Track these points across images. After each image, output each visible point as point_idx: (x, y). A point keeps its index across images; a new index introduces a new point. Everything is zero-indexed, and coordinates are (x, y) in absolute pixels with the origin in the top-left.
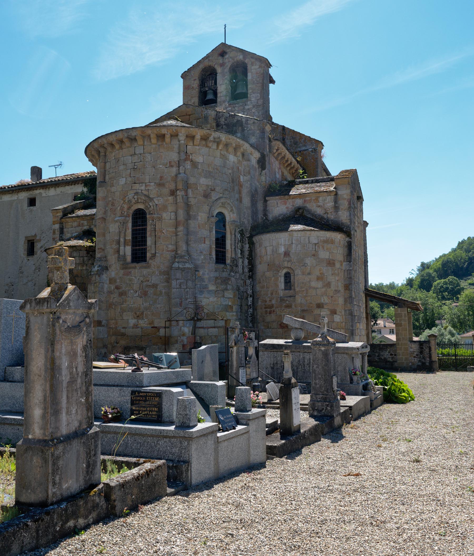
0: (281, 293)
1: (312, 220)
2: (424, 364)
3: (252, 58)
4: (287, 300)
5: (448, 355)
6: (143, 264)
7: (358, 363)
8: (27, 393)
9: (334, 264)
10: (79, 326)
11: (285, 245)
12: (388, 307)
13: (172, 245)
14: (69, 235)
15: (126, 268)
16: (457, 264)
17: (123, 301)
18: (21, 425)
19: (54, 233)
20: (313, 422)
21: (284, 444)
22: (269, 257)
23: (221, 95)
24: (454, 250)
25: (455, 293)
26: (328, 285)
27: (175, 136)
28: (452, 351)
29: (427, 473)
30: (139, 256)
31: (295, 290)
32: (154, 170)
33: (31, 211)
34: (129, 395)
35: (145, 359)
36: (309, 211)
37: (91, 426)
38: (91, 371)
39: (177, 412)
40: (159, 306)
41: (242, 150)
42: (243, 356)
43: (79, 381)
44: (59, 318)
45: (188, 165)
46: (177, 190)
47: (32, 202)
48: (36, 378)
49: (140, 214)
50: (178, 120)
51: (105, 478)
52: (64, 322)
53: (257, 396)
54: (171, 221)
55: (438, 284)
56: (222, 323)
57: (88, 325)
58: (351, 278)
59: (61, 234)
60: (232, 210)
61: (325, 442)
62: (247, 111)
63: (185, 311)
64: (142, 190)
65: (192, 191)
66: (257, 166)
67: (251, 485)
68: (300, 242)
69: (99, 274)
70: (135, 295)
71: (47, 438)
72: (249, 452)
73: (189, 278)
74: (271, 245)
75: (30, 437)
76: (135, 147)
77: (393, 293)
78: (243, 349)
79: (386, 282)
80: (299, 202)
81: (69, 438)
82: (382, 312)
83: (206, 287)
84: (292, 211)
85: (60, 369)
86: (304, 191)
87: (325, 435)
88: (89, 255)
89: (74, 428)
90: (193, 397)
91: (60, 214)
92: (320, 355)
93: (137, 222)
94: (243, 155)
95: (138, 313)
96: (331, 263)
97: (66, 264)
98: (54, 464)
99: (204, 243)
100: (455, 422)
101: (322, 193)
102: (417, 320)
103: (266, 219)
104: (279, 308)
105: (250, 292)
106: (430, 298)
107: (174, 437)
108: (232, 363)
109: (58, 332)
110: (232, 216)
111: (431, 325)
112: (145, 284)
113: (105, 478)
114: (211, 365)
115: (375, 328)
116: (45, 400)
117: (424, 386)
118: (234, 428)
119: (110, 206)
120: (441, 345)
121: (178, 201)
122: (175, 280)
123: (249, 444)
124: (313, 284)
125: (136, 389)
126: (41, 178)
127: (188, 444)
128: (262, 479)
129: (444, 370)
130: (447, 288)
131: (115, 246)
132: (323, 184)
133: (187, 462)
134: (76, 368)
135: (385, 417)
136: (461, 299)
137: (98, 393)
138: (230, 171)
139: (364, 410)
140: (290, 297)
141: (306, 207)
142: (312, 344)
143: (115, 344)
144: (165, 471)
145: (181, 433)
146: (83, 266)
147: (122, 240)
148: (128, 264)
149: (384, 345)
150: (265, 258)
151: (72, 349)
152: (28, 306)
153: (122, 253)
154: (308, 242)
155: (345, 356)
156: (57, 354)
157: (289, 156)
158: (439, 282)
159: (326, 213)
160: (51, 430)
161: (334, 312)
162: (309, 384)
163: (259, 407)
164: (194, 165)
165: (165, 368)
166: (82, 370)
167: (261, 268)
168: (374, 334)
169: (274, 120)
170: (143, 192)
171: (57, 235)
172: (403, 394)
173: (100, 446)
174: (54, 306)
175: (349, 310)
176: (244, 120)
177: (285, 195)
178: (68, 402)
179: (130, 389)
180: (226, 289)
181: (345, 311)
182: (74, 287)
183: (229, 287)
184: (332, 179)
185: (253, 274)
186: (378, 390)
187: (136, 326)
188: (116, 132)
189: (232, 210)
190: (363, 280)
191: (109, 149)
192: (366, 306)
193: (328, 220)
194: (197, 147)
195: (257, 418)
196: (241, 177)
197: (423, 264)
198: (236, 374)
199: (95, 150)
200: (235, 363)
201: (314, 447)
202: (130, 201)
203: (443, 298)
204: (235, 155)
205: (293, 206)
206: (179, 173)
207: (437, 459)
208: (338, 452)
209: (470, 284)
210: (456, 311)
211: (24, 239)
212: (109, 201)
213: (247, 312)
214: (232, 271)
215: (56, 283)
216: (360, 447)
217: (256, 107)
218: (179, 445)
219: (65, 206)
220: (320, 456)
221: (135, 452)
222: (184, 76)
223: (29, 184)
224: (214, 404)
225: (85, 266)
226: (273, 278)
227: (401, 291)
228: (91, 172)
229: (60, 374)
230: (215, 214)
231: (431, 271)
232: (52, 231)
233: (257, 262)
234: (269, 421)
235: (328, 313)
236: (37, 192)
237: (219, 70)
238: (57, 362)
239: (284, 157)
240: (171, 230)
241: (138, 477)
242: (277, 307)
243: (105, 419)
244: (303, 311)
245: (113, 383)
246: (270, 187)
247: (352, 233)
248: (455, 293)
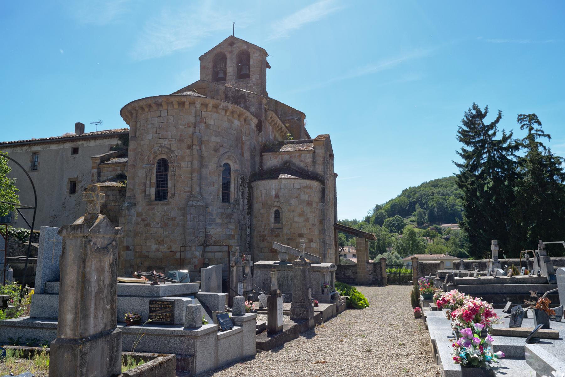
0: (272, 226)
1: (296, 171)
2: (376, 279)
5: (395, 273)
6: (165, 202)
7: (328, 279)
8: (61, 301)
9: (312, 204)
10: (107, 247)
11: (275, 189)
12: (352, 238)
14: (105, 178)
15: (151, 205)
16: (401, 206)
18: (56, 329)
19: (93, 176)
20: (293, 324)
21: (270, 340)
24: (399, 196)
25: (399, 228)
26: (307, 220)
27: (192, 103)
28: (397, 270)
29: (375, 360)
30: (161, 195)
32: (175, 129)
33: (74, 158)
34: (148, 303)
35: (162, 275)
36: (294, 164)
37: (114, 328)
38: (116, 284)
39: (186, 316)
41: (244, 116)
42: (241, 273)
43: (106, 291)
44: (90, 241)
45: (202, 126)
47: (75, 151)
48: (69, 289)
49: (163, 162)
50: (195, 92)
51: (124, 370)
52: (95, 244)
53: (251, 304)
55: (388, 221)
56: (226, 249)
57: (115, 247)
58: (324, 215)
60: (236, 162)
61: (302, 338)
62: (250, 88)
63: (197, 239)
66: (256, 129)
67: (243, 372)
69: (128, 209)
71: (76, 338)
72: (242, 347)
74: (266, 188)
75: (63, 337)
77: (355, 227)
78: (241, 268)
79: (351, 219)
80: (286, 158)
81: (95, 338)
82: (348, 241)
83: (214, 220)
85: (90, 282)
86: (290, 149)
87: (302, 334)
89: (100, 330)
90: (199, 304)
91: (98, 161)
92: (299, 273)
93: (160, 169)
94: (245, 120)
96: (309, 204)
97: (97, 198)
98: (82, 359)
100: (397, 322)
102: (373, 248)
103: (262, 169)
105: (248, 224)
106: (383, 231)
107: (183, 336)
108: (233, 279)
109: (89, 252)
111: (382, 251)
112: (165, 217)
113: (124, 370)
114: (216, 281)
115: (342, 253)
116: (76, 307)
117: (376, 296)
118: (231, 329)
120: (390, 266)
123: (243, 341)
124: (296, 219)
125: (153, 299)
126: (84, 132)
127: (194, 341)
128: (252, 368)
129: (391, 284)
130: (394, 224)
131: (142, 187)
132: (305, 144)
133: (193, 356)
134: (104, 281)
135: (347, 320)
136: (404, 232)
137: (123, 303)
138: (235, 132)
139: (331, 314)
140: (279, 228)
142: (293, 264)
144: (175, 363)
145: (189, 333)
147: (148, 182)
148: (152, 201)
149: (348, 266)
151: (100, 266)
152: (65, 231)
153: (147, 193)
155: (318, 273)
156: (88, 270)
157: (279, 122)
158: (388, 220)
159: (307, 166)
160: (80, 331)
161: (311, 240)
162: (291, 295)
163: (252, 312)
164: (207, 126)
165: (178, 282)
166: (108, 283)
167: (257, 206)
168: (341, 258)
169: (269, 96)
171: (95, 178)
172: (361, 302)
173: (121, 344)
174: (86, 232)
176: (246, 94)
177: (276, 152)
178: (96, 308)
179: (149, 299)
180: (230, 222)
181: (320, 239)
182: (104, 216)
183: (232, 221)
184: (311, 141)
185: (251, 211)
186: (342, 299)
187: (157, 251)
188: (146, 98)
189: (236, 162)
190: (333, 217)
191: (140, 111)
192: (335, 237)
193: (308, 171)
194: (210, 113)
195: (249, 321)
196: (243, 137)
197: (377, 206)
198: (235, 288)
199: (129, 112)
200: (234, 279)
201: (293, 343)
202: (155, 152)
203: (392, 231)
204: (239, 120)
206: (195, 132)
207: (383, 349)
208: (311, 346)
209: (410, 221)
210: (400, 241)
211: (67, 180)
213: (246, 240)
214: (234, 208)
215: (89, 214)
216: (328, 342)
218: (187, 342)
219: (103, 155)
220: (298, 349)
221: (151, 349)
222: (201, 58)
223: (73, 137)
224: (216, 310)
227: (362, 225)
228: (125, 129)
229: (90, 286)
230: (222, 164)
231: (383, 211)
232: (91, 174)
233: (255, 202)
234: (259, 323)
235: (307, 241)
236: (80, 143)
237: (228, 56)
238: (88, 276)
239: (276, 124)
241: (152, 368)
243: (128, 322)
244: (288, 239)
245: (135, 294)
246: (265, 145)
247: (325, 181)
248: (399, 228)
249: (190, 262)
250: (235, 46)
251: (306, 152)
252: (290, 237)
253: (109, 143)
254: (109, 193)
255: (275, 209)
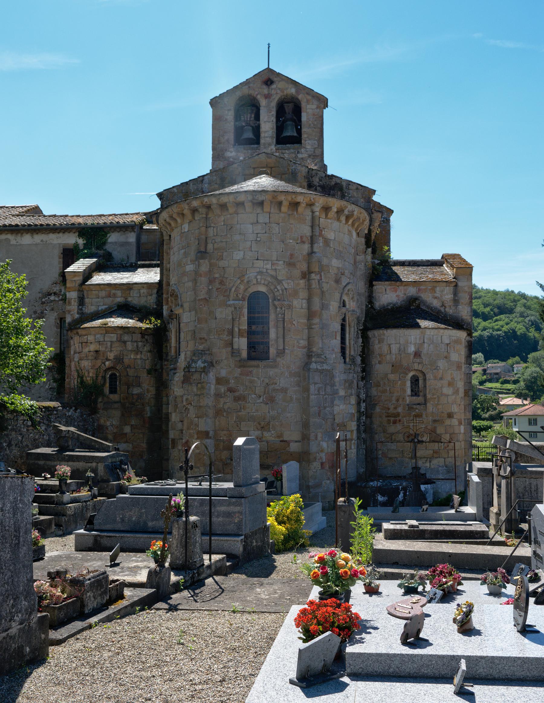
0: (408, 400)
3: (308, 94)
4: (416, 408)
11: (415, 344)
13: (303, 340)
17: (241, 408)
22: (394, 356)
23: (266, 135)
31: (425, 396)
36: (424, 303)
40: (289, 415)
46: (310, 272)
54: (302, 310)
59: (80, 305)
64: (267, 269)
65: (324, 274)
68: (433, 341)
69: (205, 370)
70: (258, 401)
73: (328, 382)
74: (394, 342)
76: (258, 214)
80: (412, 291)
84: (403, 301)
88: (144, 340)
95: (262, 423)
99: (336, 338)
101: (441, 283)
103: (372, 307)
104: (407, 418)
110: (351, 304)
112: (271, 387)
119: (217, 285)
121: (313, 286)
122: (313, 385)
131: (225, 337)
141: (421, 297)
143: (229, 461)
146: (137, 354)
150: (388, 357)
153: (236, 346)
154: (440, 342)
159: (443, 305)
164: (327, 242)
167: (380, 369)
170: (269, 271)
175: (468, 419)
205: (405, 294)
212: (215, 278)
217: (312, 157)
222: (214, 103)
225: (139, 353)
226: (399, 382)
233: (374, 361)
237: (263, 103)
240: (302, 321)
242: (405, 417)
249: (315, 458)
250: (274, 86)
251: (445, 284)
252: (437, 418)
253: (60, 241)
254: (126, 338)
255: (411, 374)
